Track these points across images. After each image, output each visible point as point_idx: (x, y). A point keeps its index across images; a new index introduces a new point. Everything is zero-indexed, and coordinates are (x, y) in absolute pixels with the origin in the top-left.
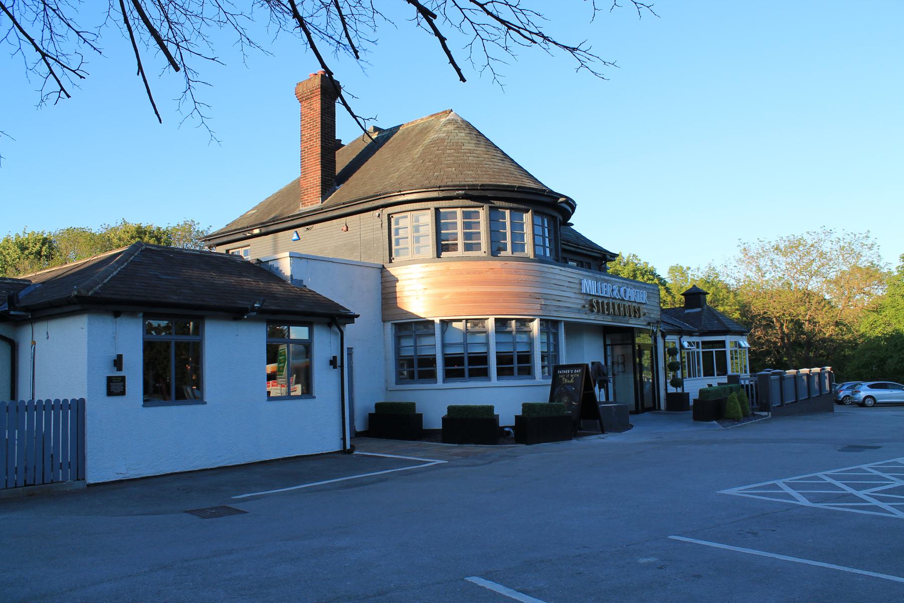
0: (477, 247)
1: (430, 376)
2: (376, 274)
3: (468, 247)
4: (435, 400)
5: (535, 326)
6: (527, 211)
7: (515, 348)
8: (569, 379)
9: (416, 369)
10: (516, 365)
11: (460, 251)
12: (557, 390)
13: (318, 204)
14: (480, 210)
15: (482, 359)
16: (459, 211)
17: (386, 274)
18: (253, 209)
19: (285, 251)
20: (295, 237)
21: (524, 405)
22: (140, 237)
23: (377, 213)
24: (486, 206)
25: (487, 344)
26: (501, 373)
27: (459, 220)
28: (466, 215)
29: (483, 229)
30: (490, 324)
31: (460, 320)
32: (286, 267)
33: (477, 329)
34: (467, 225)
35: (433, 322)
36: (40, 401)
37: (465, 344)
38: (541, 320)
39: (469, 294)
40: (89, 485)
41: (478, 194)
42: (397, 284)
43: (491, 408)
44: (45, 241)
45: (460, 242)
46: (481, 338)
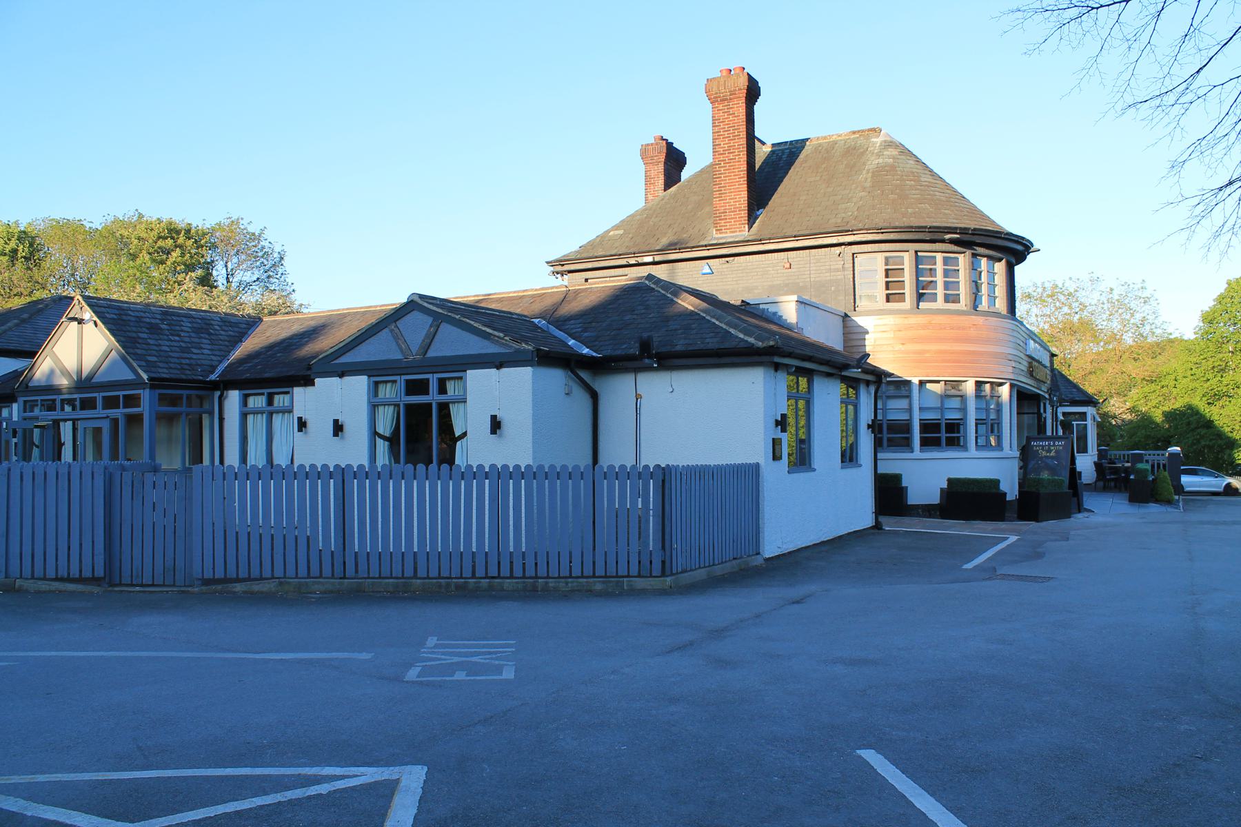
0: (901, 297)
1: (906, 444)
2: (838, 322)
3: (947, 299)
4: (926, 475)
5: (1005, 391)
6: (1000, 260)
7: (942, 415)
8: (1049, 451)
9: (885, 436)
10: (944, 435)
11: (940, 303)
12: (1032, 464)
13: (744, 233)
14: (961, 257)
15: (954, 427)
16: (939, 257)
17: (850, 324)
18: (616, 227)
19: (793, 293)
20: (707, 270)
21: (950, 481)
22: (172, 238)
23: (837, 250)
24: (969, 252)
25: (964, 409)
26: (925, 443)
27: (939, 267)
28: (946, 261)
29: (963, 278)
30: (969, 387)
31: (938, 382)
32: (789, 311)
33: (953, 392)
34: (946, 273)
35: (909, 382)
36: (302, 466)
37: (942, 409)
38: (1012, 386)
39: (915, 353)
40: (767, 560)
41: (934, 235)
42: (867, 336)
43: (997, 482)
44: (23, 236)
45: (940, 291)
46: (955, 403)
